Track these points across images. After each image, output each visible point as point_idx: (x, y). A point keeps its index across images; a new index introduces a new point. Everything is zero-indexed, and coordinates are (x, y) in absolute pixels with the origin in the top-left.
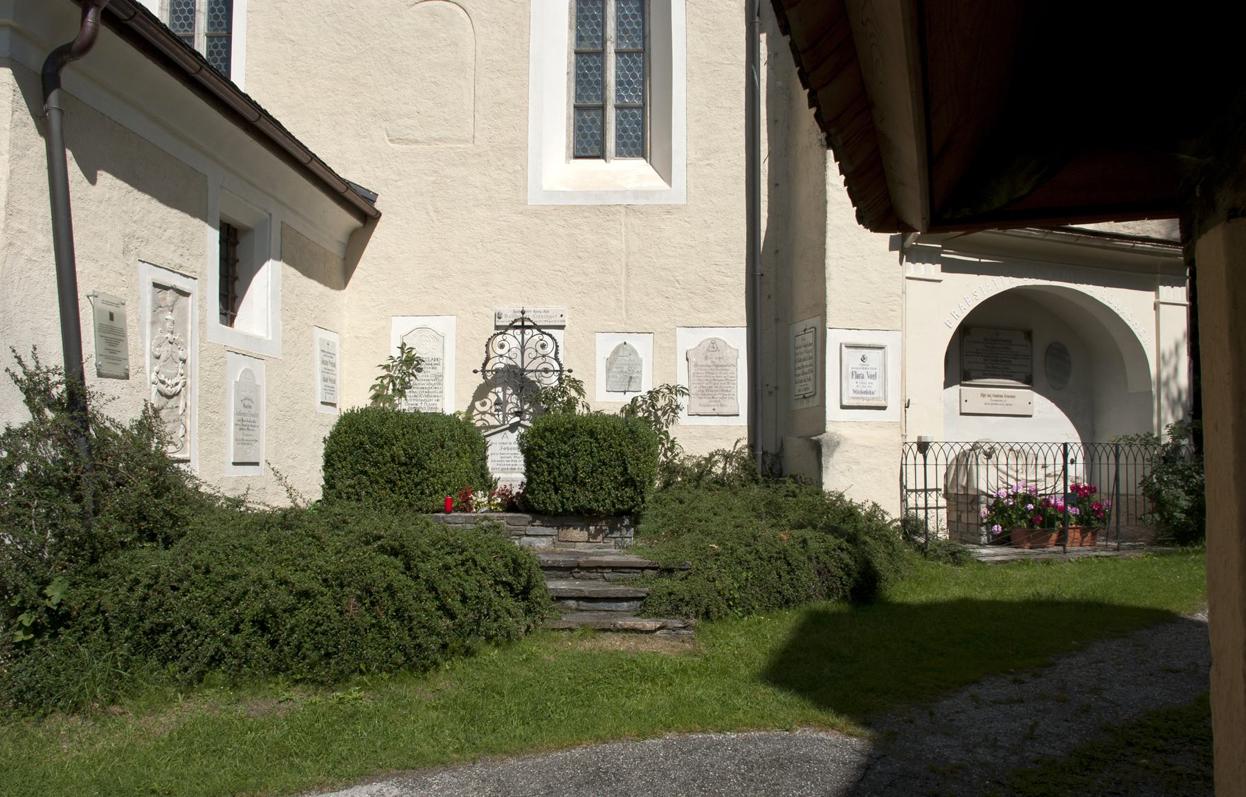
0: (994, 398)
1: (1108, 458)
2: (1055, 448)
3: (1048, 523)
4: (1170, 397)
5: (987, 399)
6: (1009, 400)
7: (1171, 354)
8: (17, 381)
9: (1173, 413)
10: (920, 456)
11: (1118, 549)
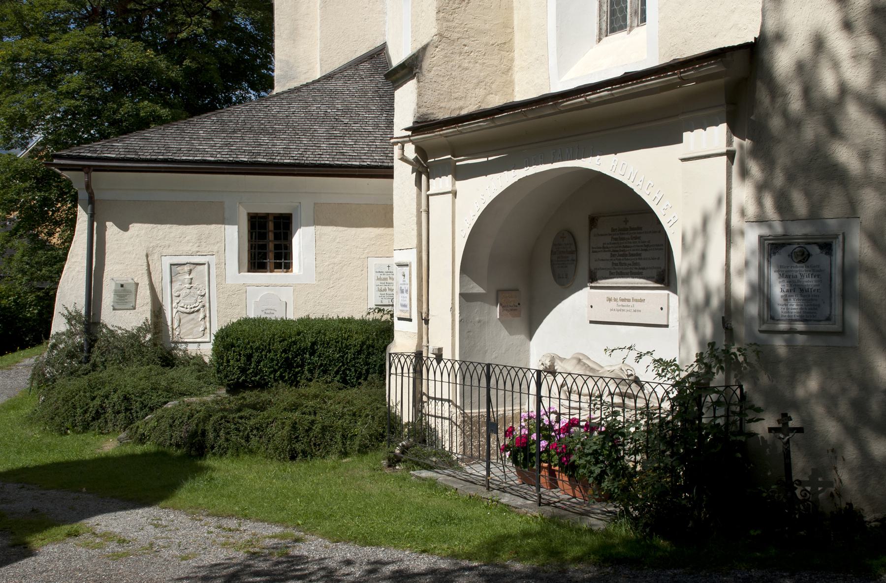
0: (621, 303)
1: (479, 381)
3: (288, 364)
4: (692, 302)
5: (613, 304)
6: (638, 306)
7: (695, 234)
8: (64, 316)
9: (696, 327)
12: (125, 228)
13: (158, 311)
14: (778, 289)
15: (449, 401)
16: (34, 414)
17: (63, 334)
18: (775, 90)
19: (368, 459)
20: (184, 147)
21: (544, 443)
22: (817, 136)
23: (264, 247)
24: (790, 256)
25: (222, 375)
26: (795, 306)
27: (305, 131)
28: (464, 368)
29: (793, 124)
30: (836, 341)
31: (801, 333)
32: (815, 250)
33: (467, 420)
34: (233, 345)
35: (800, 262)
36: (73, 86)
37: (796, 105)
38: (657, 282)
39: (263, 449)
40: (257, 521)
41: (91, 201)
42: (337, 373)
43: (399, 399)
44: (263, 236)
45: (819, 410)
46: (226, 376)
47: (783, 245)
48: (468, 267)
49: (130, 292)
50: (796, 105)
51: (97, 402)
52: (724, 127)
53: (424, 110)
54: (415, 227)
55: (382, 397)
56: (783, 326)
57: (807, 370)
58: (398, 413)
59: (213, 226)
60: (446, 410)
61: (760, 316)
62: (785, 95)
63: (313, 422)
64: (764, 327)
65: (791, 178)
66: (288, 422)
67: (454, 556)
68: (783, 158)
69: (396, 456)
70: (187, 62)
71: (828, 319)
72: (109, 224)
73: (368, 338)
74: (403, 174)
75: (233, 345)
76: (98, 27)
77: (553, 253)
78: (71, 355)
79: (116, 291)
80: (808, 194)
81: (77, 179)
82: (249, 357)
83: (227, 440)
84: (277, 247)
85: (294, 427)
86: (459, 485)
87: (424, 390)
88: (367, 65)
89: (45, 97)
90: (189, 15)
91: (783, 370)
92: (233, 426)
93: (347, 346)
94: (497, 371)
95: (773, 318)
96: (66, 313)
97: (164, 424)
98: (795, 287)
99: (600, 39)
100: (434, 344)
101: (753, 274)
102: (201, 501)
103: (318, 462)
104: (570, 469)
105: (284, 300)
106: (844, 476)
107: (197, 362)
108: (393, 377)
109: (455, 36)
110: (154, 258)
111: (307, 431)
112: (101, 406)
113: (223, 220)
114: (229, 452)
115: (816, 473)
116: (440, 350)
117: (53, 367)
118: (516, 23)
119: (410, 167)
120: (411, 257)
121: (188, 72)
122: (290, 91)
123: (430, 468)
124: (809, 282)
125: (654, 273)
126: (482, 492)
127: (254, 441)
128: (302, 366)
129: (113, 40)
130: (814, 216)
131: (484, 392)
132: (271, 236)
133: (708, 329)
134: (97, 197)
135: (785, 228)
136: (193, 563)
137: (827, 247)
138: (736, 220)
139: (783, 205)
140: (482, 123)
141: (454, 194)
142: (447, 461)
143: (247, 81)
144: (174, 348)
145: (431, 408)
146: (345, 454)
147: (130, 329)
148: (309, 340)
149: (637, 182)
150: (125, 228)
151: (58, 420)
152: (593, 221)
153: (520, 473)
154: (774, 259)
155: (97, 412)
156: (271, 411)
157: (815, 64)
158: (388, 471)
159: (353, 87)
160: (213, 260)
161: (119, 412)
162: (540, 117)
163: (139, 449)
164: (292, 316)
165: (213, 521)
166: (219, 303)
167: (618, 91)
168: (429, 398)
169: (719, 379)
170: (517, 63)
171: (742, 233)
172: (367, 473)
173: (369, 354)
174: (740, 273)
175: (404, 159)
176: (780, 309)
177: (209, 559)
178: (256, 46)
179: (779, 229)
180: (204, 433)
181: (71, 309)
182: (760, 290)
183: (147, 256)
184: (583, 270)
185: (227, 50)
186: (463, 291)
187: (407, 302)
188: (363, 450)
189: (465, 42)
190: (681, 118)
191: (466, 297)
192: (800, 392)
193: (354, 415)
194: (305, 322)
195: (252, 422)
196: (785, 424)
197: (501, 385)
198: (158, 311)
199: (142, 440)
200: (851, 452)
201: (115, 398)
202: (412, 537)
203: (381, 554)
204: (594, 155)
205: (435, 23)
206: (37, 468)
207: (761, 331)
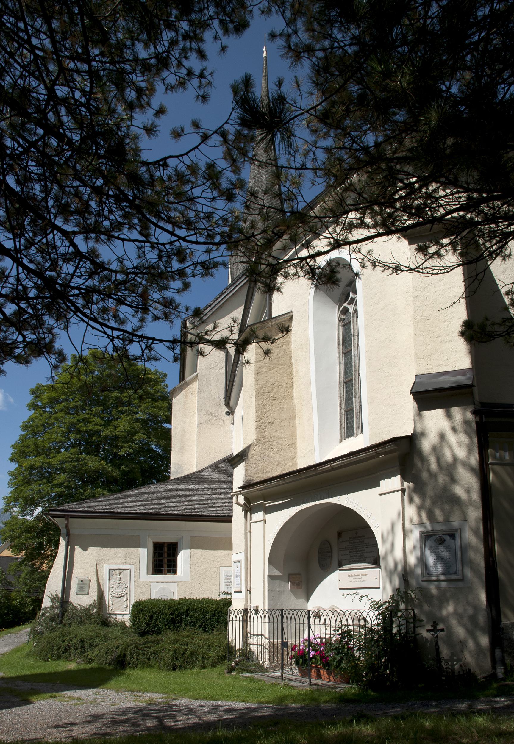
2: (277, 613)
3: (173, 622)
5: (351, 578)
6: (364, 578)
7: (388, 533)
9: (391, 582)
10: (255, 616)
11: (336, 688)
12: (85, 549)
13: (101, 596)
14: (431, 559)
15: (261, 635)
16: (30, 651)
17: (48, 607)
18: (423, 459)
19: (218, 669)
20: (120, 505)
21: (312, 653)
22: (444, 480)
23: (161, 561)
24: (435, 541)
25: (136, 627)
26: (440, 568)
27: (186, 498)
28: (269, 613)
29: (433, 476)
30: (460, 584)
31: (443, 581)
32: (447, 538)
33: (272, 646)
34: (142, 610)
35: (440, 544)
36: (61, 480)
37: (434, 466)
38: (373, 564)
39: (157, 665)
40: (153, 692)
41: (68, 534)
42: (200, 626)
43: (234, 637)
44: (161, 555)
45: (454, 622)
46: (138, 628)
47: (431, 536)
48: (272, 561)
49: (86, 585)
50: (434, 466)
51: (66, 643)
52: (399, 477)
53: (249, 478)
54: (244, 540)
55: (226, 637)
56: (434, 578)
57: (447, 601)
58: (233, 645)
59: (133, 549)
60: (260, 640)
61: (422, 573)
62: (428, 461)
63: (186, 650)
64: (424, 579)
65: (434, 502)
66: (172, 649)
67: (260, 703)
68: (430, 492)
69: (232, 667)
70: (123, 467)
71: (456, 573)
72: (76, 547)
73: (218, 607)
74: (238, 512)
75: (142, 610)
76: (77, 449)
77: (319, 553)
78: (52, 619)
79: (78, 584)
80: (442, 510)
81: (60, 522)
82: (151, 617)
83: (137, 659)
84: (169, 561)
85: (175, 652)
86: (267, 679)
87: (248, 630)
88: (222, 465)
89: (45, 487)
90: (125, 442)
91: (436, 602)
92: (141, 652)
93: (206, 612)
94: (287, 613)
95: (429, 574)
96: (51, 596)
97: (103, 652)
98: (439, 558)
99: (341, 441)
100: (254, 605)
101: (418, 553)
102: (122, 685)
103: (188, 671)
104: (327, 665)
105: (172, 590)
106: (469, 658)
107: (122, 625)
108: (231, 622)
109: (266, 440)
110: (100, 566)
111: (182, 654)
112: (68, 645)
113: (138, 546)
114: (139, 666)
115: (453, 655)
116: (257, 607)
117: (42, 626)
118: (298, 434)
119: (241, 508)
120: (241, 557)
121: (123, 473)
122: (179, 478)
123: (250, 672)
124: (446, 554)
125: (372, 560)
126: (280, 681)
127: (152, 660)
128: (181, 623)
129: (84, 456)
130: (447, 521)
131: (280, 625)
132: (166, 555)
133: (397, 582)
134: (71, 532)
135: (432, 527)
136: (117, 707)
137: (452, 536)
138: (408, 525)
139: (431, 516)
140: (278, 482)
141: (265, 521)
142: (261, 668)
143: (155, 479)
144: (109, 617)
145: (252, 640)
146: (204, 667)
147: (85, 606)
148: (185, 608)
149: (359, 508)
150: (85, 549)
151: (44, 653)
152: (339, 534)
153: (300, 671)
154: (428, 543)
155: (66, 649)
156: (163, 644)
157: (441, 446)
158: (227, 675)
159: (214, 476)
160: (132, 568)
161: (77, 649)
162: (308, 477)
163: (88, 666)
164: (176, 598)
165: (128, 694)
166: (135, 592)
167: (346, 461)
168: (251, 635)
169: (402, 607)
170: (299, 455)
171: (411, 531)
172: (215, 676)
173: (219, 616)
174: (411, 552)
175: (238, 504)
176: (432, 569)
177: (125, 706)
178: (161, 460)
179: (429, 527)
180: (125, 655)
181: (53, 594)
182: (422, 560)
183: (96, 565)
184: (335, 562)
185: (145, 462)
186: (270, 574)
187: (239, 582)
188: (214, 665)
189: (271, 443)
190: (379, 473)
191: (271, 577)
192: (444, 613)
193: (209, 646)
194: (185, 600)
195: (152, 649)
196: (435, 627)
197: (289, 621)
198: (101, 596)
199: (90, 661)
200: (471, 644)
201: (75, 641)
202: (237, 696)
203: (219, 703)
204: (337, 496)
205: (255, 434)
206: (32, 675)
207: (423, 581)
